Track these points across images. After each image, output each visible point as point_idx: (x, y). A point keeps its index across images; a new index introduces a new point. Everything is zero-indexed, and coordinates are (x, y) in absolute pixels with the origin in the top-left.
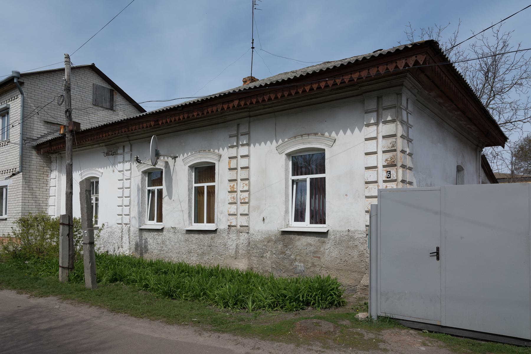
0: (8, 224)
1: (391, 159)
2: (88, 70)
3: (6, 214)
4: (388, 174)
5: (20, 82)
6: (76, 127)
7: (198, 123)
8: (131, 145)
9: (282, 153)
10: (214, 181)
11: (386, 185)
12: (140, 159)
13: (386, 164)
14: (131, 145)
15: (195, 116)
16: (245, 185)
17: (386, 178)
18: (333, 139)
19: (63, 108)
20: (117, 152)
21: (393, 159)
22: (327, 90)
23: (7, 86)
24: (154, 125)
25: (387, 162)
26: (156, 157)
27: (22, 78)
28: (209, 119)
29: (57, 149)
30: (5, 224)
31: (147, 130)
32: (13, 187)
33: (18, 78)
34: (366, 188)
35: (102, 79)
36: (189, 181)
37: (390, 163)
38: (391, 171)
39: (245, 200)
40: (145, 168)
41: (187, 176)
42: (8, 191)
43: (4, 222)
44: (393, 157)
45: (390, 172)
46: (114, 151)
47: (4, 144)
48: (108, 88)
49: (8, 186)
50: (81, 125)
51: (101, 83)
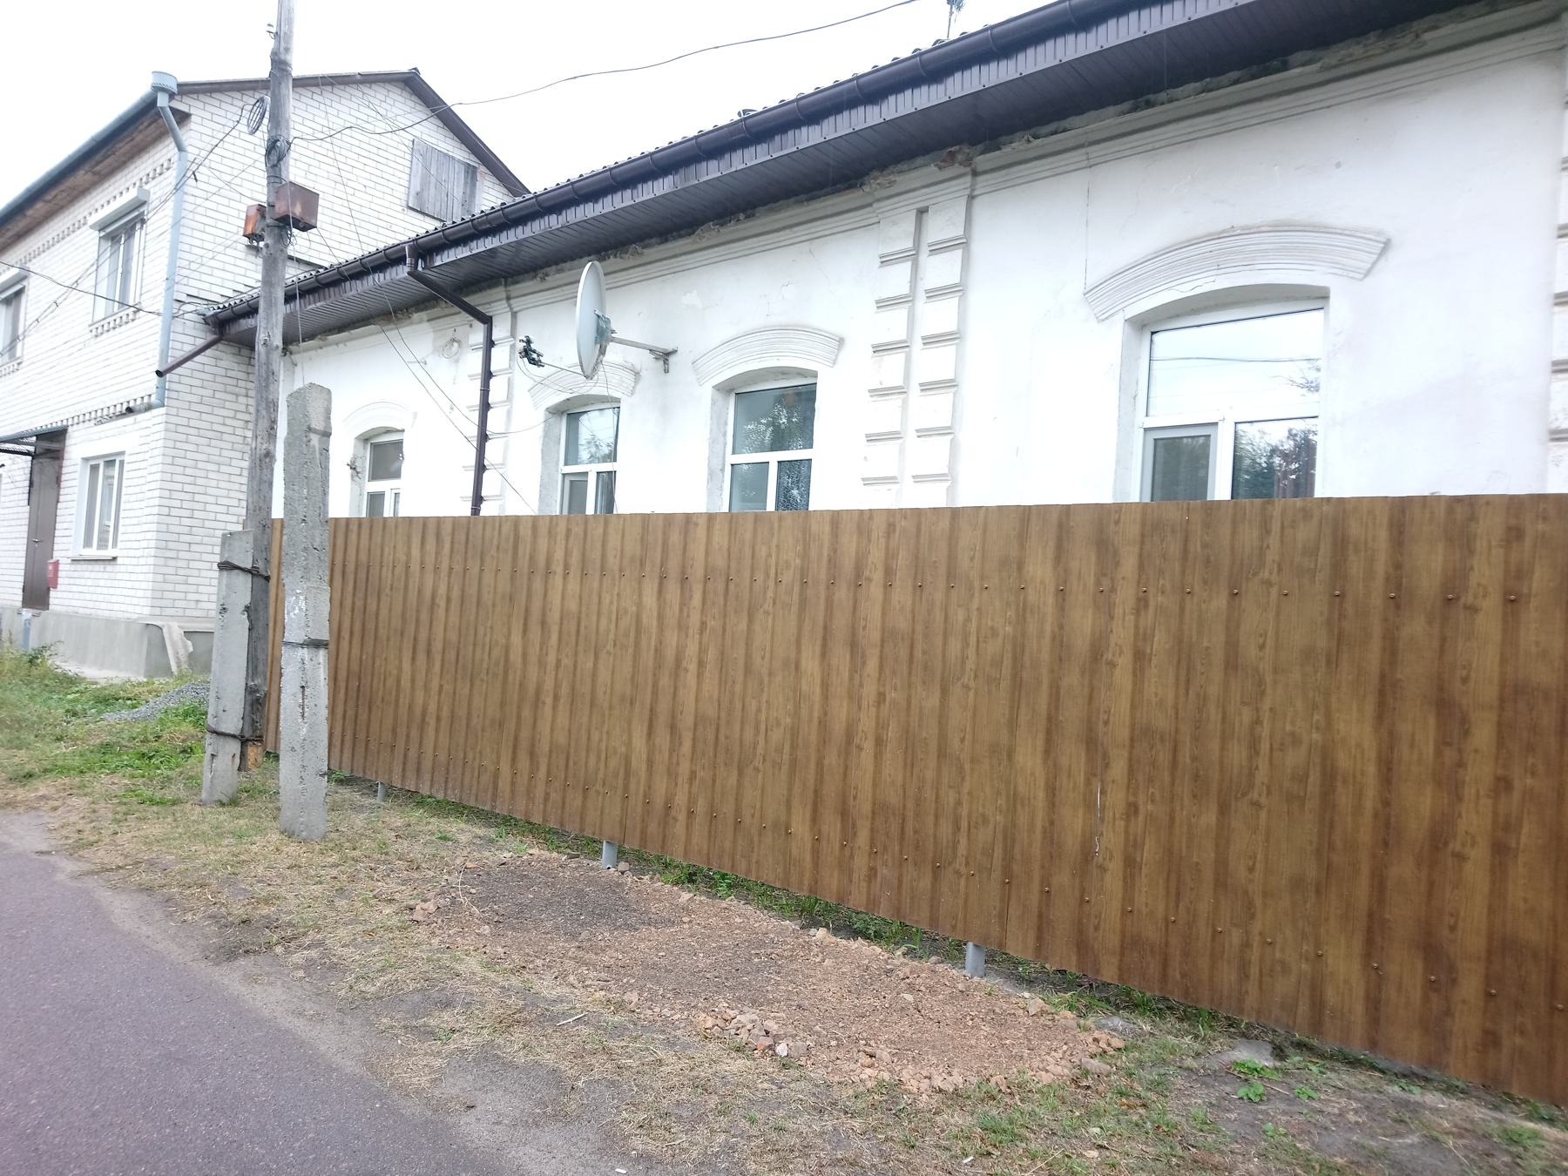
0: (119, 576)
2: (399, 91)
3: (115, 545)
5: (178, 110)
6: (303, 208)
8: (514, 315)
9: (1112, 315)
10: (809, 444)
12: (538, 350)
14: (514, 315)
18: (1378, 239)
19: (262, 136)
23: (141, 127)
26: (596, 343)
27: (185, 99)
30: (113, 575)
32: (141, 457)
33: (172, 96)
36: (713, 442)
41: (709, 422)
42: (125, 469)
43: (109, 568)
47: (124, 318)
49: (127, 453)
50: (321, 202)
51: (438, 136)
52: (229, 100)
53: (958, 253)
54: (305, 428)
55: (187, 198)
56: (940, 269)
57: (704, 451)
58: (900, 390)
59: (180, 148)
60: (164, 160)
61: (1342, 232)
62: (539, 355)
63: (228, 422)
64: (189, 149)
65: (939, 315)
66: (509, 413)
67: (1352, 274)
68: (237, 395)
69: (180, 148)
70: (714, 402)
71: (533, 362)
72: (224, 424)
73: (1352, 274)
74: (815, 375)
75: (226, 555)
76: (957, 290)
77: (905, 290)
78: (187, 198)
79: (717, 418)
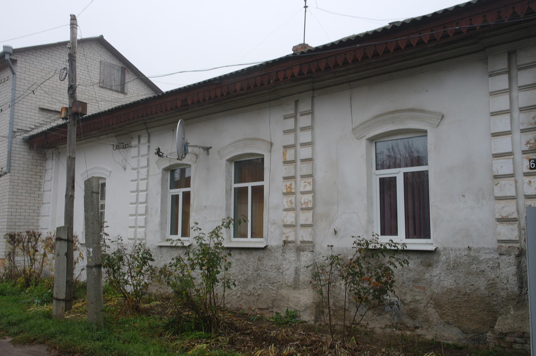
4: (531, 164)
12: (162, 152)
13: (526, 148)
16: (307, 183)
20: (131, 144)
25: (529, 145)
33: (10, 54)
46: (126, 143)
52: (31, 53)
53: (310, 116)
54: (91, 191)
55: (16, 92)
56: (304, 121)
57: (224, 184)
58: (293, 162)
59: (14, 73)
60: (5, 77)
61: (430, 112)
62: (163, 154)
63: (33, 177)
64: (17, 73)
65: (305, 137)
66: (148, 171)
67: (433, 126)
68: (37, 166)
69: (14, 73)
70: (226, 165)
71: (160, 156)
72: (32, 178)
73: (433, 126)
74: (263, 155)
75: (59, 235)
76: (311, 128)
77: (293, 127)
78: (16, 92)
79: (228, 172)
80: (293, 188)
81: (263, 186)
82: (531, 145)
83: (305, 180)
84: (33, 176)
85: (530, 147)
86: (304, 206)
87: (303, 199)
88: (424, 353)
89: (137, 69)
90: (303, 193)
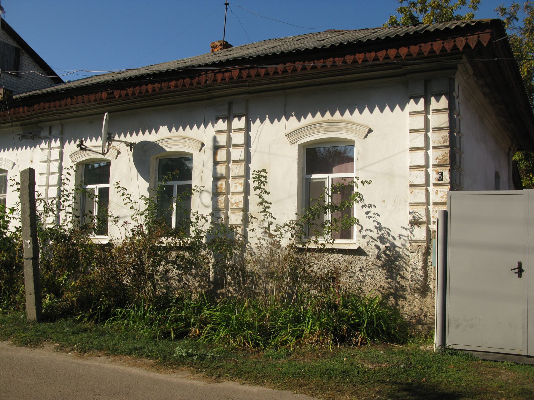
1: (443, 158)
4: (439, 176)
7: (169, 99)
8: (62, 126)
11: (436, 189)
13: (436, 163)
14: (62, 126)
15: (180, 87)
16: (238, 184)
17: (436, 180)
20: (40, 135)
21: (445, 157)
22: (60, 108)
24: (107, 99)
25: (438, 160)
28: (187, 94)
29: (50, 108)
31: (90, 105)
34: (411, 193)
35: (5, 33)
37: (442, 162)
38: (443, 172)
39: (238, 205)
40: (84, 157)
44: (446, 155)
45: (442, 173)
46: (35, 133)
48: (13, 46)
80: (223, 188)
81: (108, 188)
82: (440, 160)
83: (237, 181)
84: (219, 159)
85: (439, 162)
86: (234, 207)
87: (234, 199)
88: (386, 325)
89: (34, 51)
90: (233, 193)
